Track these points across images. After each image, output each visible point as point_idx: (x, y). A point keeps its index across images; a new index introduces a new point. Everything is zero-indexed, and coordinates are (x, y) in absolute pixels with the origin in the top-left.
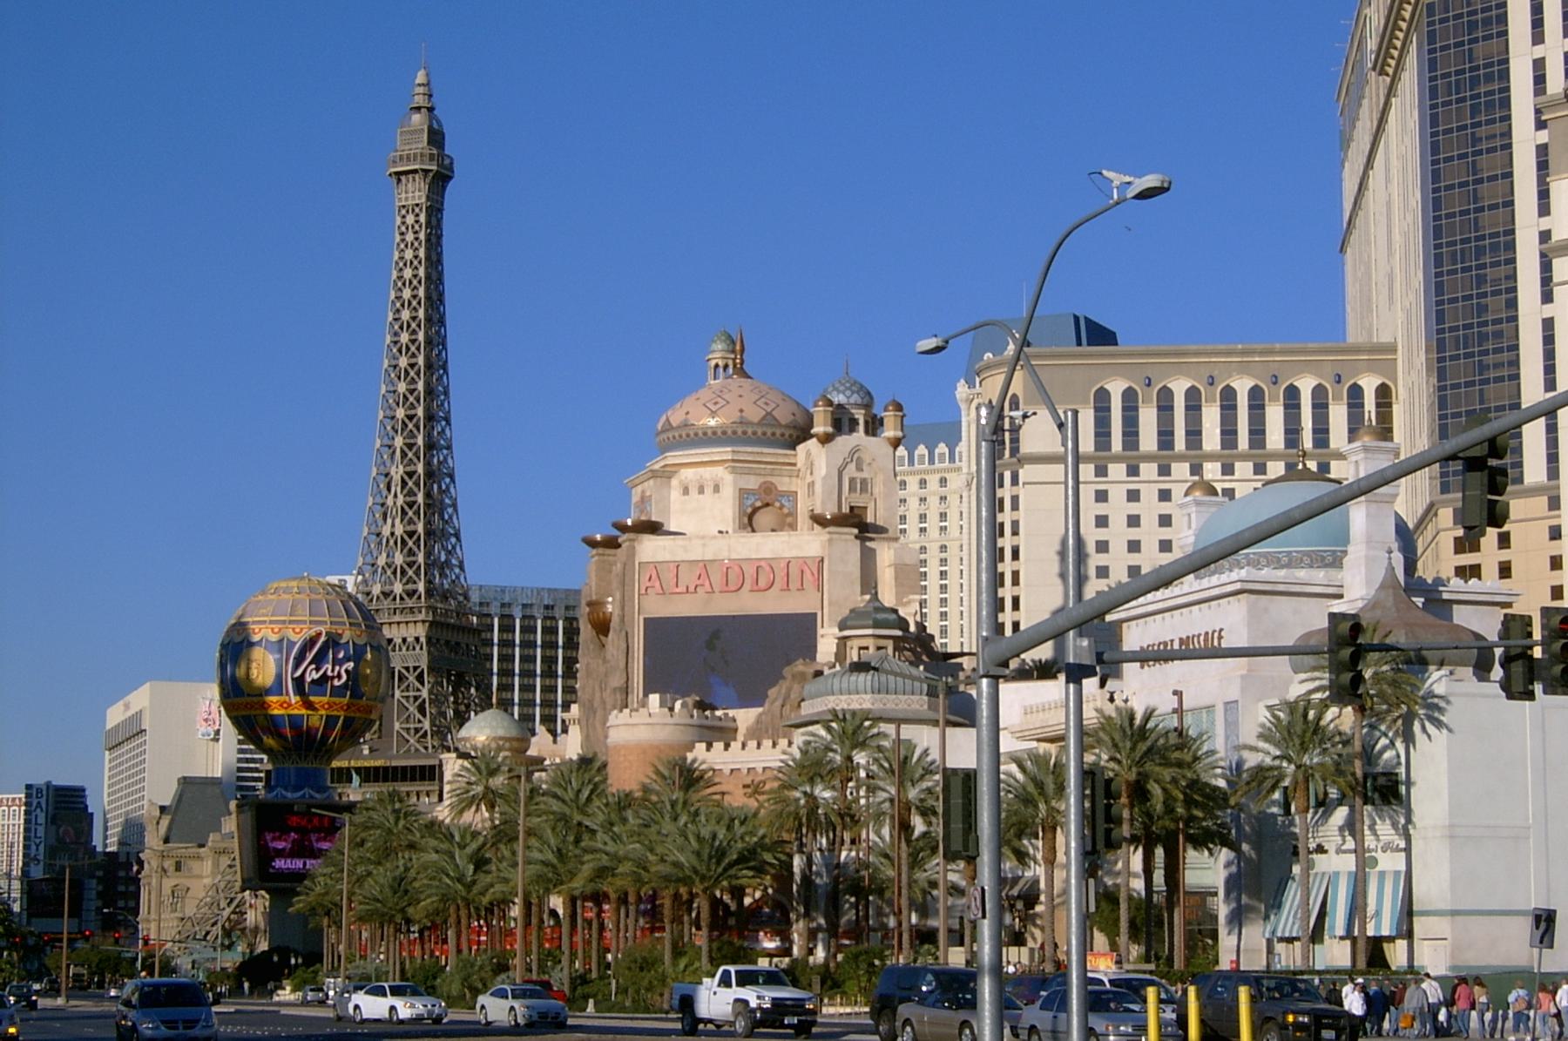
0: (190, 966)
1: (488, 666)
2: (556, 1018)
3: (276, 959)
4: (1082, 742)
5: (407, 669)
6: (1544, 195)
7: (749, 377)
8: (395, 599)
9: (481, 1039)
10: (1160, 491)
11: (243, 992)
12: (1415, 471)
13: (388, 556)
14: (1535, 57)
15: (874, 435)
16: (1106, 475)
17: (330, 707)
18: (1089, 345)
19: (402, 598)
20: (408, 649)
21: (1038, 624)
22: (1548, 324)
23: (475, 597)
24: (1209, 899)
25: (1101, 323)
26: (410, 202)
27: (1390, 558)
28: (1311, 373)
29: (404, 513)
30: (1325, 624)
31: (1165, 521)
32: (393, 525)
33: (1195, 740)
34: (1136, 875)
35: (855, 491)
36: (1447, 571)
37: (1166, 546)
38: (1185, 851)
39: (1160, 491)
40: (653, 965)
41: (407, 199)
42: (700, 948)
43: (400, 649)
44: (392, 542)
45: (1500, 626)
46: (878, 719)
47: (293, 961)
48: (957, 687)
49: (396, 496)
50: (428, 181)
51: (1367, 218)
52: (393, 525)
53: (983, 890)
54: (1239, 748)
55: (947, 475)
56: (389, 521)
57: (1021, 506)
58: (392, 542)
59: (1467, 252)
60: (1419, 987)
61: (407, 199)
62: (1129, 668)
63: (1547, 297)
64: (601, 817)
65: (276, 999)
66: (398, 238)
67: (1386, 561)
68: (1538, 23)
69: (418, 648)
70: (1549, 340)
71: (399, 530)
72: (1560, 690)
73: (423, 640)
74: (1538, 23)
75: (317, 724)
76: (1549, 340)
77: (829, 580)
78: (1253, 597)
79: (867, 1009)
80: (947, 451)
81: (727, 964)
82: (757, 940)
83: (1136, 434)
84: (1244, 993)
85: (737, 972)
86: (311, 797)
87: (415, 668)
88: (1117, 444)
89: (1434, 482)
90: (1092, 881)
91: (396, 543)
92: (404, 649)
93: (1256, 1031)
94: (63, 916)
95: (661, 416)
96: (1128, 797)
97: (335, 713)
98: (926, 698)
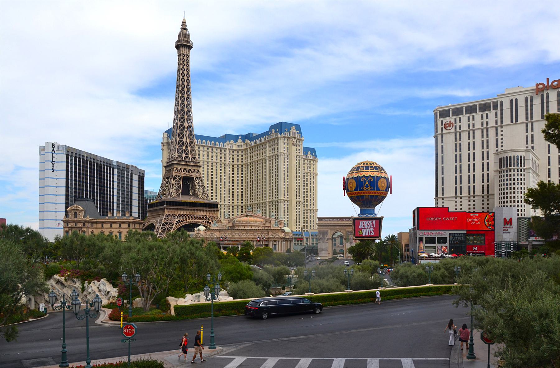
5: (176, 176)
6: (442, 141)
7: (184, 27)
8: (183, 158)
10: (447, 237)
18: (435, 237)
19: (184, 158)
20: (177, 171)
24: (548, 128)
25: (474, 349)
26: (186, 53)
27: (53, 166)
30: (408, 232)
31: (474, 205)
32: (186, 139)
36: (219, 202)
37: (461, 209)
39: (447, 237)
40: (536, 356)
44: (186, 144)
46: (252, 241)
49: (186, 131)
50: (223, 290)
52: (186, 139)
54: (542, 117)
56: (185, 138)
57: (454, 155)
58: (186, 144)
59: (372, 169)
60: (374, 243)
62: (534, 210)
63: (442, 164)
64: (522, 313)
67: (54, 166)
70: (443, 169)
71: (188, 141)
76: (443, 169)
84: (448, 359)
86: (368, 216)
87: (179, 176)
88: (472, 194)
89: (492, 193)
90: (289, 247)
98: (412, 228)
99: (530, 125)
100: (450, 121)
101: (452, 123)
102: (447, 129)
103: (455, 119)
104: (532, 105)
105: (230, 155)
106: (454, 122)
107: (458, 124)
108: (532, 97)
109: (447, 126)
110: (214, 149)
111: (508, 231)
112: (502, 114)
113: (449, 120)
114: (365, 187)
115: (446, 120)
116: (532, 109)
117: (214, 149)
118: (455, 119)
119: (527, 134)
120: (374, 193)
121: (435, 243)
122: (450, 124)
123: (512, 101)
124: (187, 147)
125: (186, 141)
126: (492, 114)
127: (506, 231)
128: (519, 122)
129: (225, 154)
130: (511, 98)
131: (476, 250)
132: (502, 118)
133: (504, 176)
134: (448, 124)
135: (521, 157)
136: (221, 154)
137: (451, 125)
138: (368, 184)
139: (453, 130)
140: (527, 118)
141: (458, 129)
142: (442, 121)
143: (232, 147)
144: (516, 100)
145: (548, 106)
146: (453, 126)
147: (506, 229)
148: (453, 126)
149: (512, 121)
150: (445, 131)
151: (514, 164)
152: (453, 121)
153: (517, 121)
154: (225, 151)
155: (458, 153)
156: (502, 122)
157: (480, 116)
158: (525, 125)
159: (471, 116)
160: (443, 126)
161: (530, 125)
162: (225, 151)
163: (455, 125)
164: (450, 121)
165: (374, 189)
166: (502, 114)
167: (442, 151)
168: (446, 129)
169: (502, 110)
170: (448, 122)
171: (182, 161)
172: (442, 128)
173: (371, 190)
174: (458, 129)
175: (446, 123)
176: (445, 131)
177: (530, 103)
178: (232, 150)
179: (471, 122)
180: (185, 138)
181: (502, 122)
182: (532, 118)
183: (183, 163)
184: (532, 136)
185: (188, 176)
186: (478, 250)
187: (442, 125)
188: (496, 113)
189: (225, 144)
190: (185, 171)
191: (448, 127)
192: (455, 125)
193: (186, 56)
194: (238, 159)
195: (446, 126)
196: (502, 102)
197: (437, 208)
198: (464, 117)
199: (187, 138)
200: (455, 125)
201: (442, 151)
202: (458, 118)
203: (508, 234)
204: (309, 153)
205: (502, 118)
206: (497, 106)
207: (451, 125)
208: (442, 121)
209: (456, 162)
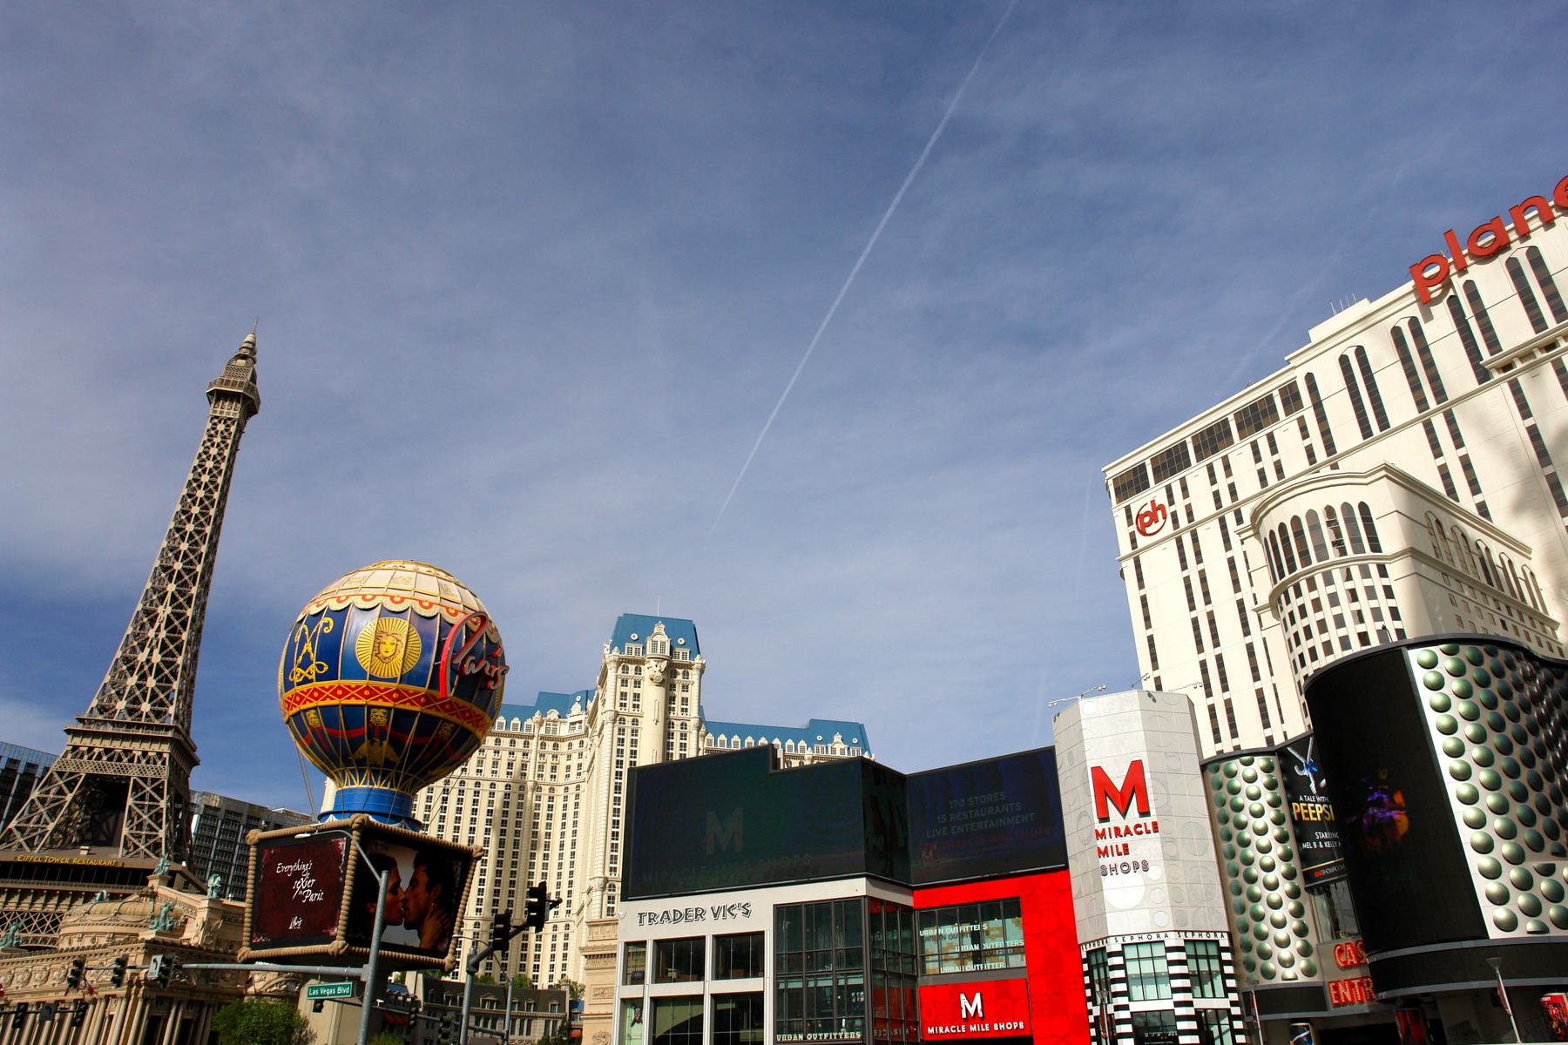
0: (107, 977)
1: (372, 910)
2: (522, 985)
3: (296, 923)
4: (716, 1007)
5: (145, 780)
8: (141, 716)
9: (614, 627)
10: (762, 933)
11: (788, 979)
12: (1226, 909)
13: (140, 679)
14: (1269, 729)
15: (1412, 317)
16: (1547, 328)
17: (452, 708)
18: (370, 947)
19: (147, 716)
20: (148, 762)
21: (889, 769)
22: (1151, 639)
23: (308, 1029)
28: (1296, 908)
29: (164, 646)
33: (614, 661)
34: (846, 981)
35: (895, 927)
38: (388, 723)
39: (762, 933)
41: (221, 413)
42: (364, 983)
43: (139, 761)
45: (245, 430)
47: (379, 1001)
48: (149, 983)
51: (1342, 576)
53: (1265, 539)
55: (569, 923)
56: (147, 650)
61: (221, 413)
63: (1141, 586)
65: (1314, 340)
66: (206, 438)
68: (1216, 731)
69: (160, 762)
72: (1155, 1021)
73: (166, 756)
74: (1216, 731)
75: (383, 721)
77: (284, 643)
78: (922, 891)
79: (1346, 875)
80: (739, 740)
81: (327, 664)
82: (457, 664)
83: (1188, 596)
85: (758, 997)
91: (157, 643)
92: (144, 761)
93: (1264, 1043)
94: (119, 846)
95: (397, 559)
96: (125, 973)
97: (408, 707)
99: (1439, 423)
100: (1153, 502)
101: (1162, 507)
102: (1149, 530)
103: (1169, 489)
104: (1424, 350)
105: (542, 755)
106: (1166, 503)
107: (1180, 506)
108: (1413, 322)
109: (1147, 519)
110: (517, 740)
111: (1129, 859)
112: (1321, 418)
113: (1148, 500)
114: (299, 666)
115: (1139, 503)
116: (1429, 364)
117: (517, 740)
118: (1169, 489)
119: (1440, 461)
120: (390, 695)
121: (700, 976)
122: (1155, 512)
123: (1344, 360)
124: (143, 677)
125: (148, 661)
126: (1285, 430)
127: (1119, 860)
128: (1394, 423)
129: (525, 754)
130: (1338, 352)
131: (972, 1019)
132: (1326, 433)
133: (1309, 635)
134: (1147, 514)
135: (1330, 511)
136: (512, 753)
137: (1159, 513)
138: (311, 649)
139: (1169, 529)
140: (1421, 403)
141: (1183, 521)
142: (1128, 510)
143: (555, 730)
144: (1360, 351)
145: (1487, 329)
146: (1165, 518)
147: (1120, 841)
148: (1165, 518)
149: (1366, 432)
150: (1142, 541)
151: (1304, 554)
152: (1162, 499)
153: (1383, 423)
154: (526, 744)
155: (1201, 611)
156: (1330, 447)
157: (1249, 449)
158: (1420, 427)
159: (1216, 460)
160: (1133, 528)
161: (1439, 423)
162: (526, 744)
163: (1173, 508)
164: (1153, 502)
165: (331, 675)
166: (1321, 418)
167: (1147, 619)
168: (1144, 534)
169: (1318, 406)
170: (1149, 508)
171: (139, 726)
172: (1132, 535)
173: (319, 678)
174: (1183, 521)
175: (1142, 512)
176: (1142, 541)
177: (1417, 346)
178: (550, 739)
179: (1222, 484)
180: (147, 650)
181: (1330, 447)
182: (1440, 393)
183: (140, 732)
184: (1466, 464)
185: (110, 772)
186: (990, 1013)
187: (1130, 524)
188: (1301, 420)
189: (529, 722)
190: (125, 760)
191: (1149, 525)
192: (1169, 510)
193: (225, 422)
194: (568, 768)
195: (1143, 522)
196: (1310, 378)
197: (697, 756)
198: (1196, 475)
199: (156, 651)
200: (1173, 508)
201: (1147, 619)
202: (1174, 482)
203: (1135, 877)
204: (837, 738)
205: (1326, 433)
206: (1297, 396)
207: (1159, 513)
208: (1128, 510)
209: (1219, 658)
